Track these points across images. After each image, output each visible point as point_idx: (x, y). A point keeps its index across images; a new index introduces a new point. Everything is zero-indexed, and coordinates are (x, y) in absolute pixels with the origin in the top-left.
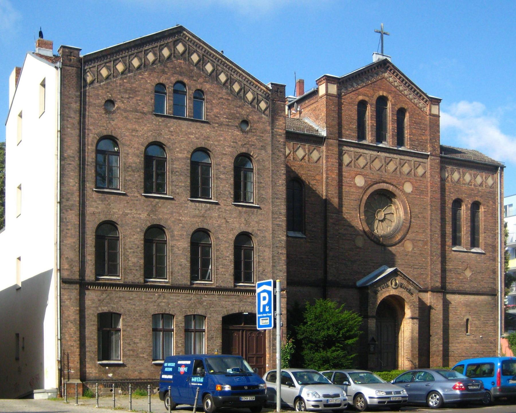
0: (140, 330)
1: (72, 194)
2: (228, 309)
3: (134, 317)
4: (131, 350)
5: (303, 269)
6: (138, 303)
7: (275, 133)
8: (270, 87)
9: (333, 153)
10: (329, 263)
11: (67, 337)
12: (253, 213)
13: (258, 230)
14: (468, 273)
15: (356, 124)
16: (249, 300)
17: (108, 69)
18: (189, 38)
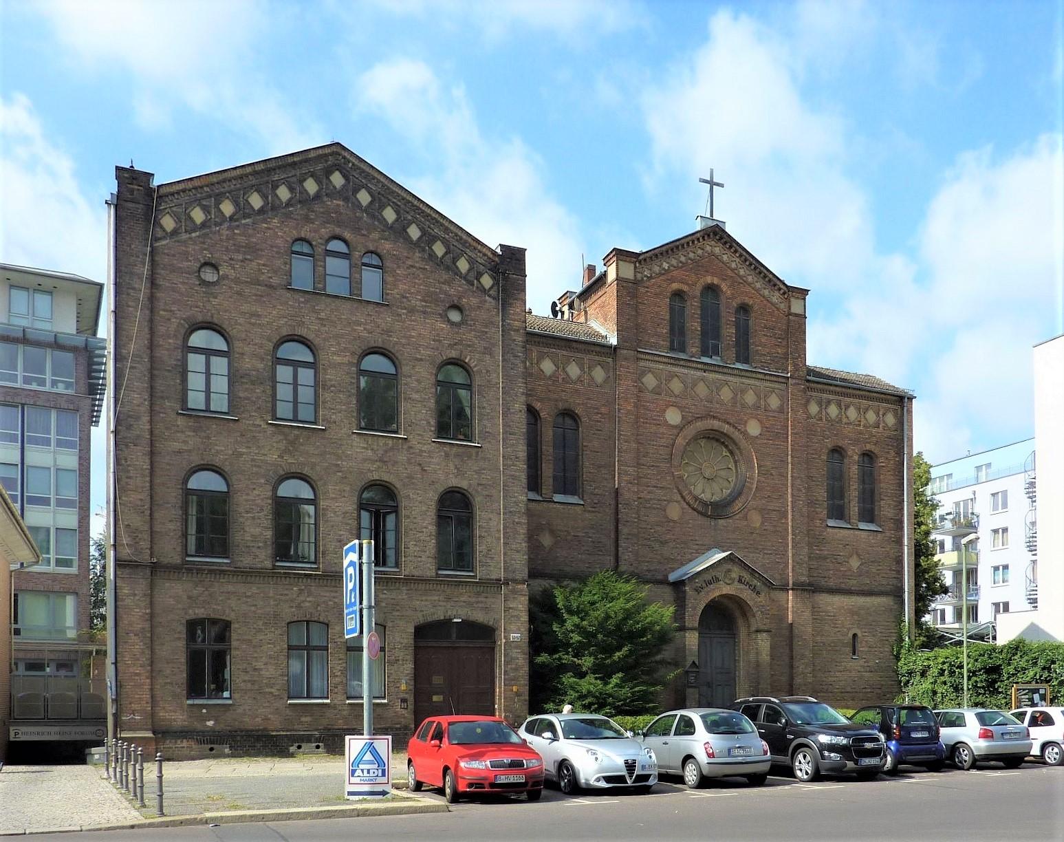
0: (265, 648)
1: (138, 418)
2: (425, 613)
3: (255, 626)
4: (249, 681)
5: (579, 554)
6: (261, 603)
7: (508, 327)
8: (499, 251)
9: (629, 372)
10: (622, 543)
11: (127, 659)
12: (470, 457)
13: (479, 484)
14: (855, 563)
15: (668, 328)
17: (206, 209)
18: (353, 164)
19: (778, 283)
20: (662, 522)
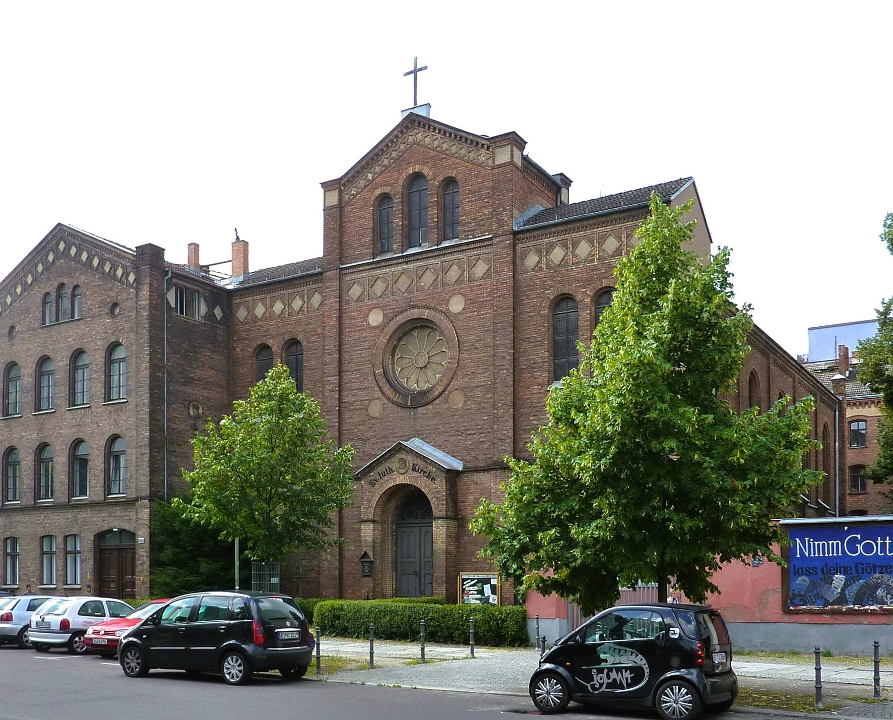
16: (117, 514)
19: (479, 140)
20: (364, 421)
